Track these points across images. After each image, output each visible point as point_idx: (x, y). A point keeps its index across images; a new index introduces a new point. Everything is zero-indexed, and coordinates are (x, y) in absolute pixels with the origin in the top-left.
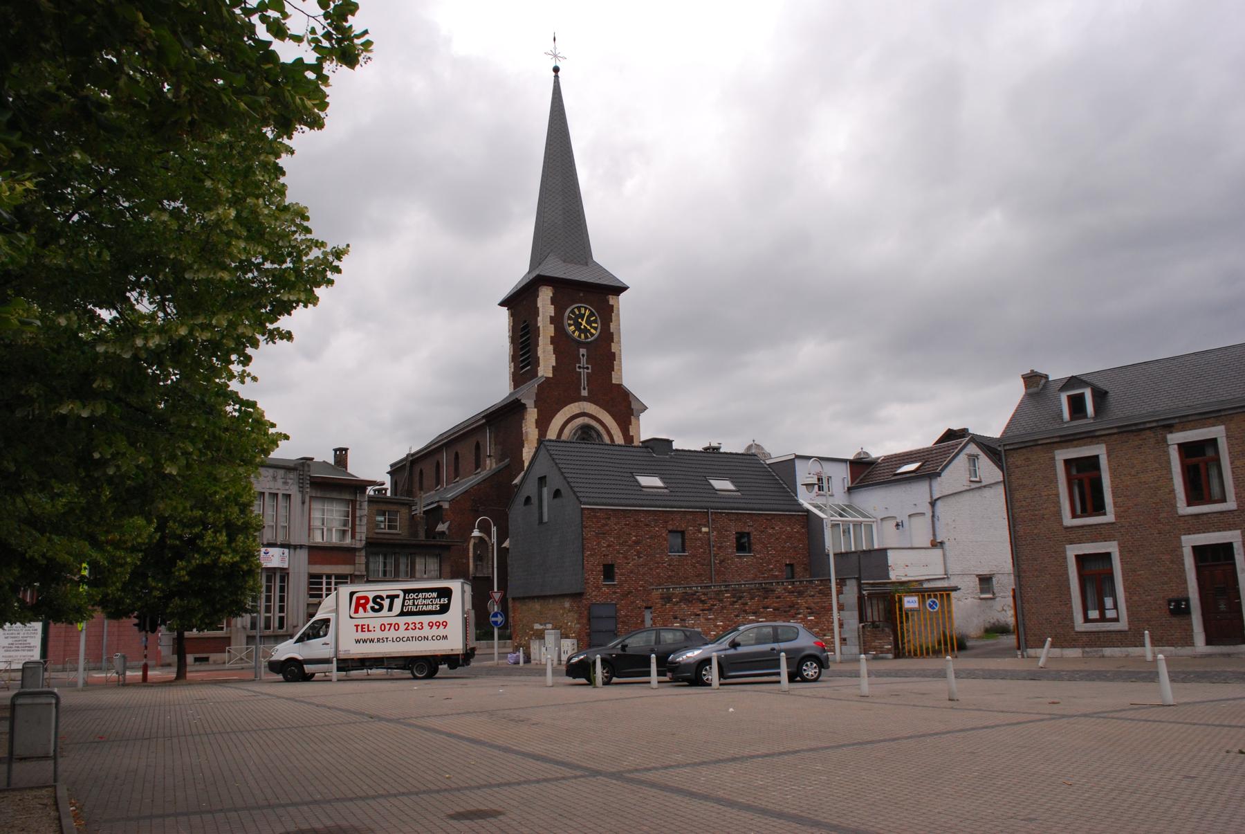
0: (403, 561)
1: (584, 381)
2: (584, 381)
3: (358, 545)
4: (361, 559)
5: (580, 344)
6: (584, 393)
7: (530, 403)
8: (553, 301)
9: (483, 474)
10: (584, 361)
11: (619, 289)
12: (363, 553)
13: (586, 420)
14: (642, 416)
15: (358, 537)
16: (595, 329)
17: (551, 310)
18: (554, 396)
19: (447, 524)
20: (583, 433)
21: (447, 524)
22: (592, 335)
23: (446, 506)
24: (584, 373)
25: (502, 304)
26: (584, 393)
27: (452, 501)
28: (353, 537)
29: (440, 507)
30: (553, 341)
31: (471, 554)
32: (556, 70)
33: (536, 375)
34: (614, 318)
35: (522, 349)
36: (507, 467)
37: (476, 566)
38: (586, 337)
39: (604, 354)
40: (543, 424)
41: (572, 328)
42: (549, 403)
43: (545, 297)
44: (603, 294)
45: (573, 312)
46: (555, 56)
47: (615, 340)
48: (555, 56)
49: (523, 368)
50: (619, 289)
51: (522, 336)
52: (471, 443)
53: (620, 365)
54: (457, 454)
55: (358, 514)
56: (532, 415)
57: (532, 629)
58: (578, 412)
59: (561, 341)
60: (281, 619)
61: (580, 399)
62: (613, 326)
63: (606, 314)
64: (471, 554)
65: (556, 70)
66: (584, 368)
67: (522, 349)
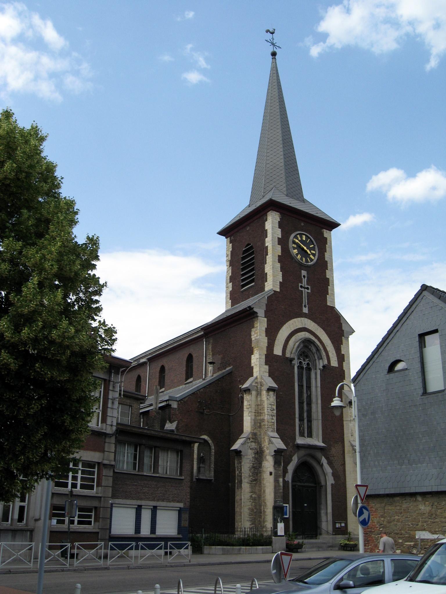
0: (147, 453)
1: (305, 300)
2: (305, 300)
3: (109, 430)
4: (110, 446)
5: (302, 266)
6: (305, 310)
7: (261, 312)
9: (196, 384)
10: (305, 281)
11: (332, 225)
12: (113, 440)
14: (351, 338)
15: (109, 422)
16: (314, 255)
18: (281, 308)
19: (175, 424)
20: (305, 347)
21: (175, 424)
22: (312, 260)
23: (175, 405)
24: (305, 292)
25: (221, 233)
26: (305, 310)
27: (182, 401)
28: (104, 420)
29: (168, 406)
31: (195, 456)
32: (274, 54)
33: (262, 289)
34: (327, 249)
35: (243, 269)
36: (230, 373)
37: (199, 468)
38: (307, 261)
40: (271, 333)
42: (277, 316)
43: (272, 223)
44: (320, 226)
45: (296, 237)
46: (273, 44)
47: (329, 267)
48: (273, 44)
49: (243, 286)
50: (332, 225)
51: (243, 258)
52: (183, 355)
53: (333, 290)
54: (163, 369)
55: (110, 397)
57: (412, 538)
58: (300, 326)
59: (285, 259)
60: (22, 509)
61: (301, 315)
62: (327, 255)
63: (323, 244)
64: (195, 456)
65: (274, 54)
66: (305, 288)
67: (243, 269)
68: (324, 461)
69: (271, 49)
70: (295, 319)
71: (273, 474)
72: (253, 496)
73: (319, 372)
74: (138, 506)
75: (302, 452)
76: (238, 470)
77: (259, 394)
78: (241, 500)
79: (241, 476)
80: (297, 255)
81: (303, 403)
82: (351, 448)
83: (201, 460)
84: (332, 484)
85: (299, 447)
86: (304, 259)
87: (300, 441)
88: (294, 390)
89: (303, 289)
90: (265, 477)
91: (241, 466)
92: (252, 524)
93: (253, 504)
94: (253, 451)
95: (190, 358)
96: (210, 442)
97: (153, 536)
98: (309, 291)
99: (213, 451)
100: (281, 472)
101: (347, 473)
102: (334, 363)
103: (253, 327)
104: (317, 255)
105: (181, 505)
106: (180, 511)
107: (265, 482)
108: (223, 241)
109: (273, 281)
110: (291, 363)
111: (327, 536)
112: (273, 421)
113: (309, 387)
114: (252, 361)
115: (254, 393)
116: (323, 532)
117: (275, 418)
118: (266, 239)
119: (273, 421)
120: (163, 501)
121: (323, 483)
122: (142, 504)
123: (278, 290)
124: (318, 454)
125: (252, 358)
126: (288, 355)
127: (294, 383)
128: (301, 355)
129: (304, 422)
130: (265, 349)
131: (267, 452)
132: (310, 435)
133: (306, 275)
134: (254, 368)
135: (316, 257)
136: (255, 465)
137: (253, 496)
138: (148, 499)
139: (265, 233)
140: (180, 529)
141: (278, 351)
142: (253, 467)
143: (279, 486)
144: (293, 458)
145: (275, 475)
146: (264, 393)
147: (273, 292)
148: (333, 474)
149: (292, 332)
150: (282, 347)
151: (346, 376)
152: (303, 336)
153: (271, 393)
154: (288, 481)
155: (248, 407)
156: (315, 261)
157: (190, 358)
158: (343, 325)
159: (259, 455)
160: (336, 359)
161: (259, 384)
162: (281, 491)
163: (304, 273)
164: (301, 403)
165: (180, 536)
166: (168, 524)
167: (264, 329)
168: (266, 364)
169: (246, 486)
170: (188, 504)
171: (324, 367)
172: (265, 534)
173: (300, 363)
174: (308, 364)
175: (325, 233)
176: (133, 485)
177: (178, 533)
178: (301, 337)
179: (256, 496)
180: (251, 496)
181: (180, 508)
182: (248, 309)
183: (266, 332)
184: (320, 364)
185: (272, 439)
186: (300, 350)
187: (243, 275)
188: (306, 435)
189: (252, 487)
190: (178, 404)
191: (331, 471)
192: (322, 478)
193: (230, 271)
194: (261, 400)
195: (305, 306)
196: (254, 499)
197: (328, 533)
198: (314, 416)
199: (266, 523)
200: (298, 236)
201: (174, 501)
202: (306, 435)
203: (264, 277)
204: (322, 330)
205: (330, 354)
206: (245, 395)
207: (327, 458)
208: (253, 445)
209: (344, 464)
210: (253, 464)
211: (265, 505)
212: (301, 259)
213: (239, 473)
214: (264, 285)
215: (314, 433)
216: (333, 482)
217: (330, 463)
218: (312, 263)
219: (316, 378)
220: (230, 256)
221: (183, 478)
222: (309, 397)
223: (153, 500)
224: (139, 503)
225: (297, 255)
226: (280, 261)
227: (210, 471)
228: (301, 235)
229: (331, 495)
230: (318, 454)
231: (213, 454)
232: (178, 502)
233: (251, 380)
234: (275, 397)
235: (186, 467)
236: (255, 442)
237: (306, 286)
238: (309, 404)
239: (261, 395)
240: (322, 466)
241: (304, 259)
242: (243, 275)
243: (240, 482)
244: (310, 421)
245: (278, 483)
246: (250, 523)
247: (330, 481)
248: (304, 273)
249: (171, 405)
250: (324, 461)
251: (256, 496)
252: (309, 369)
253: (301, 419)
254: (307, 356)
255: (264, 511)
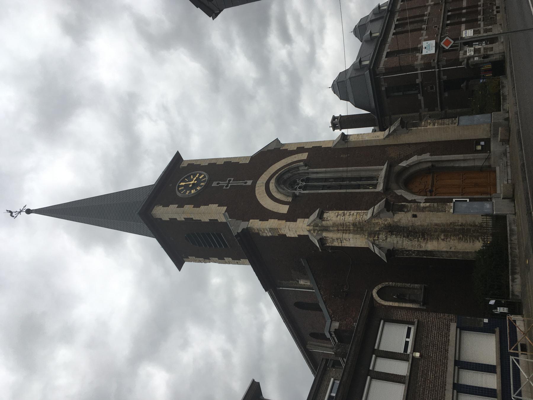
1: (241, 183)
2: (241, 183)
6: (249, 183)
8: (166, 205)
10: (222, 183)
11: (178, 158)
13: (272, 186)
14: (282, 142)
16: (200, 175)
17: (173, 207)
18: (244, 204)
23: (336, 325)
24: (233, 183)
29: (336, 331)
30: (197, 205)
31: (396, 304)
32: (29, 212)
39: (220, 171)
41: (193, 191)
45: (180, 191)
46: (20, 212)
49: (226, 246)
50: (178, 158)
56: (256, 224)
59: (197, 201)
63: (195, 167)
64: (396, 304)
65: (29, 212)
68: (404, 164)
69: (24, 214)
70: (256, 192)
71: (415, 213)
72: (442, 237)
73: (311, 170)
74: (454, 388)
75: (393, 185)
76: (411, 255)
77: (326, 229)
78: (447, 252)
79: (418, 251)
80: (196, 190)
81: (341, 185)
82: (391, 137)
83: (401, 298)
84: (431, 155)
85: (387, 188)
86: (202, 184)
87: (380, 188)
88: (326, 193)
89: (230, 185)
90: (419, 223)
91: (407, 251)
92: (478, 239)
93: (452, 238)
94: (389, 236)
95: (299, 305)
96: (380, 286)
97: (499, 370)
98: (232, 179)
99: (390, 283)
100: (413, 205)
101: (418, 140)
102: (304, 156)
103: (258, 234)
104: (200, 172)
105: (453, 326)
106: (462, 328)
107: (426, 224)
108: (186, 265)
109: (215, 212)
110: (298, 196)
111: (492, 159)
112: (355, 214)
113: (326, 180)
114: (293, 236)
115: (325, 234)
116: (487, 164)
117: (352, 212)
118: (178, 219)
119: (355, 214)
120: (447, 351)
121: (430, 165)
122: (452, 382)
123: (225, 208)
124: (397, 169)
125: (290, 236)
126: (290, 199)
127: (318, 193)
128: (293, 187)
129: (361, 185)
130: (280, 222)
131: (389, 220)
132: (376, 178)
133: (217, 182)
134: (299, 234)
135: (202, 172)
136: (405, 235)
137: (442, 237)
138: (445, 372)
139: (173, 221)
140: (487, 330)
141: (284, 209)
142: (408, 237)
143: (430, 206)
144: (399, 194)
145: (417, 211)
146: (324, 223)
147: (226, 213)
148: (420, 154)
149: (268, 195)
150: (281, 205)
151: (318, 145)
152: (273, 184)
153: (325, 215)
154: (425, 199)
155: (339, 241)
156: (204, 173)
157: (299, 305)
158: (269, 149)
159: (393, 229)
160: (301, 154)
161: (316, 228)
162: (435, 205)
163: (214, 184)
164: (341, 187)
165: (497, 330)
166: (483, 347)
167: (261, 222)
168: (296, 221)
169: (431, 246)
170: (452, 316)
171: (306, 165)
172: (490, 223)
173: (300, 188)
174: (302, 181)
175: (183, 166)
176: (423, 393)
177: (493, 332)
178: (274, 187)
179: (443, 234)
180: (443, 240)
181: (457, 327)
182: (239, 238)
183: (263, 221)
184: (303, 169)
185: (374, 214)
186: (287, 188)
187: (216, 246)
188: (375, 182)
189: (432, 239)
190: (335, 321)
191: (416, 156)
192: (425, 166)
193: (214, 259)
194: (333, 227)
195: (246, 183)
196: (446, 237)
197: (488, 159)
198: (355, 174)
199: (477, 224)
200: (180, 189)
201: (447, 335)
202: (375, 182)
203: (214, 222)
204: (271, 168)
205: (295, 160)
206: (328, 245)
207: (401, 161)
208: (382, 236)
209: (409, 144)
210: (404, 237)
211: (406, 193)
212: (201, 186)
213: (414, 253)
214: (221, 222)
215: (374, 174)
216: (429, 154)
217: (407, 158)
218: (207, 177)
219: (317, 173)
220: (201, 259)
221: (416, 321)
222: (336, 179)
223: (445, 365)
224: (449, 387)
225: (196, 190)
226: (198, 206)
227: (414, 288)
228: (179, 186)
229: (443, 156)
230: (397, 169)
231: (394, 284)
232: (448, 330)
233: (311, 238)
234: (330, 212)
235: (401, 315)
236: (379, 234)
237: (227, 182)
238: (343, 179)
239: (327, 227)
240: (410, 166)
241: (202, 184)
242: (216, 246)
243: (426, 252)
244: (361, 179)
245: (425, 208)
246: (477, 241)
247: (426, 157)
248: (214, 184)
249: (335, 329)
250: (404, 164)
251: (443, 234)
252: (308, 180)
253: (359, 187)
254: (295, 182)
255: (461, 225)
